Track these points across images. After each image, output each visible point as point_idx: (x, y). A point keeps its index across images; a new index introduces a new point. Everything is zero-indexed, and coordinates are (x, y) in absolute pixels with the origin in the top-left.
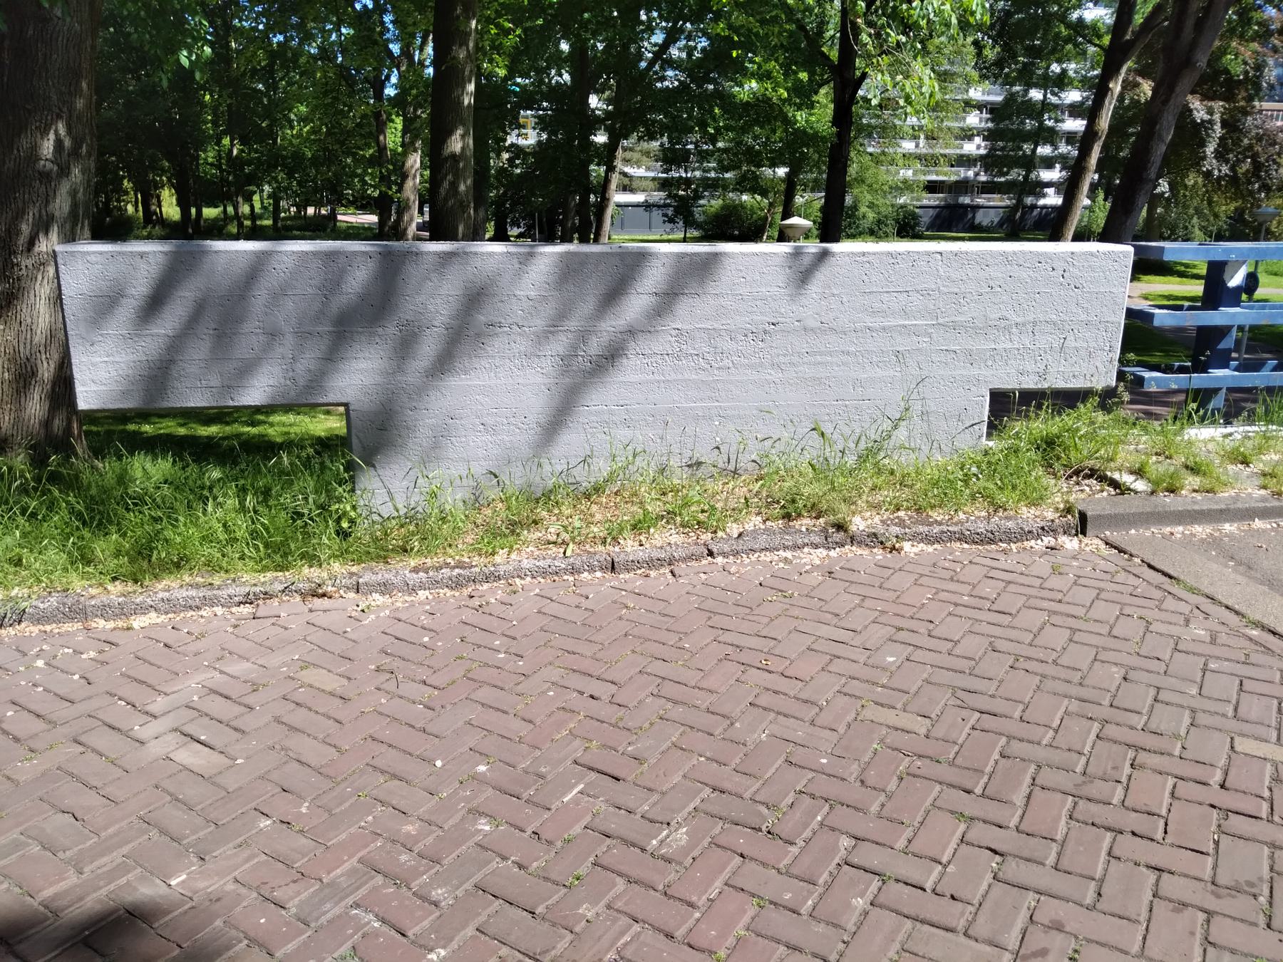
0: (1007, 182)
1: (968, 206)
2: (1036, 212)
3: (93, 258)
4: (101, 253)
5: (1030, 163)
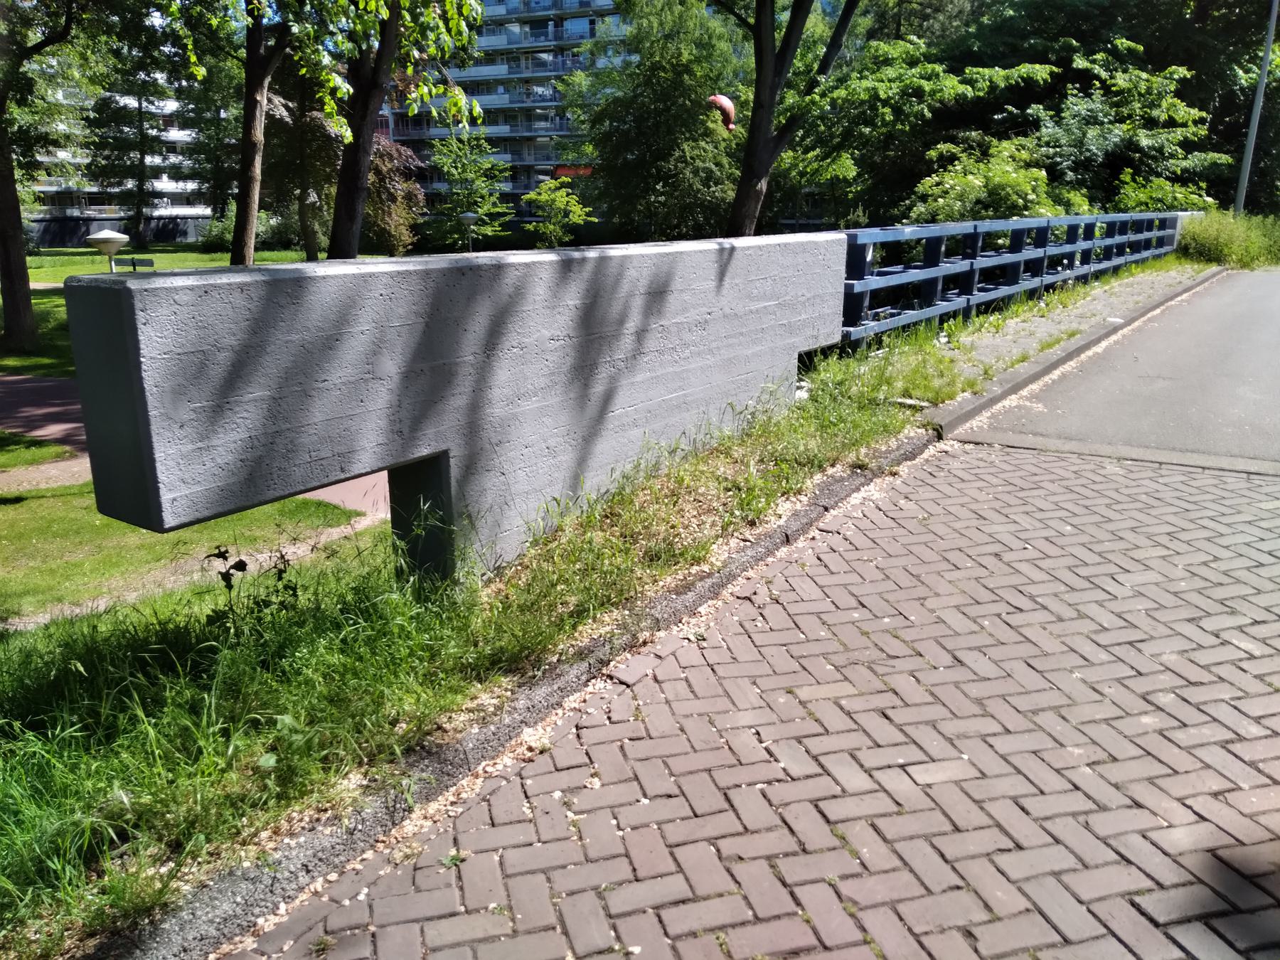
0: (122, 193)
1: (77, 219)
2: (153, 224)
3: (183, 298)
4: (191, 289)
5: (143, 174)
